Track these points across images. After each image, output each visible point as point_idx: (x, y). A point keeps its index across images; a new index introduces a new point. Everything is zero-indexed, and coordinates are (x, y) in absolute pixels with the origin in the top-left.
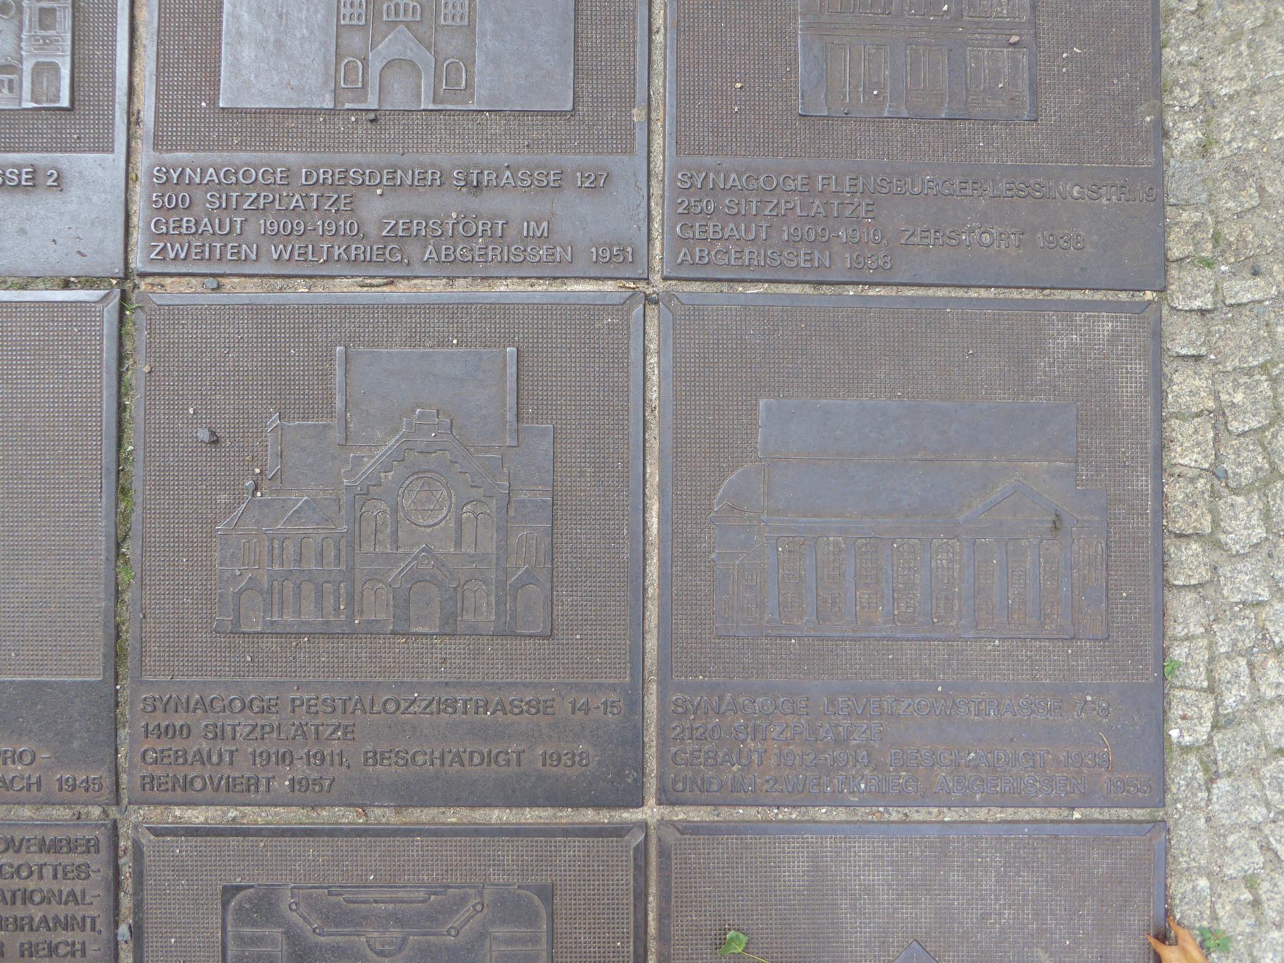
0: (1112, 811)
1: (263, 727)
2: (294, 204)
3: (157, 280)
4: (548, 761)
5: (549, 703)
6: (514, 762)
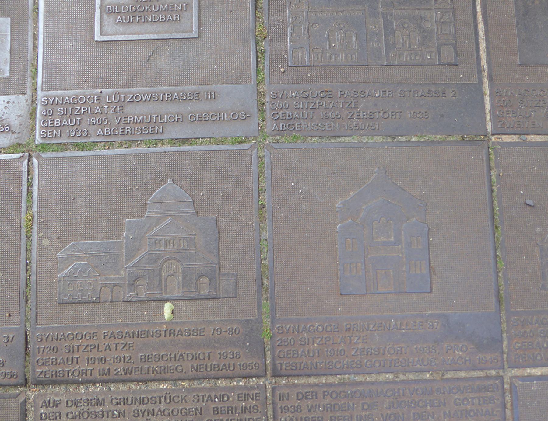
0: (373, 380)
1: (91, 346)
2: (96, 111)
3: (499, 136)
4: (116, 361)
5: (202, 331)
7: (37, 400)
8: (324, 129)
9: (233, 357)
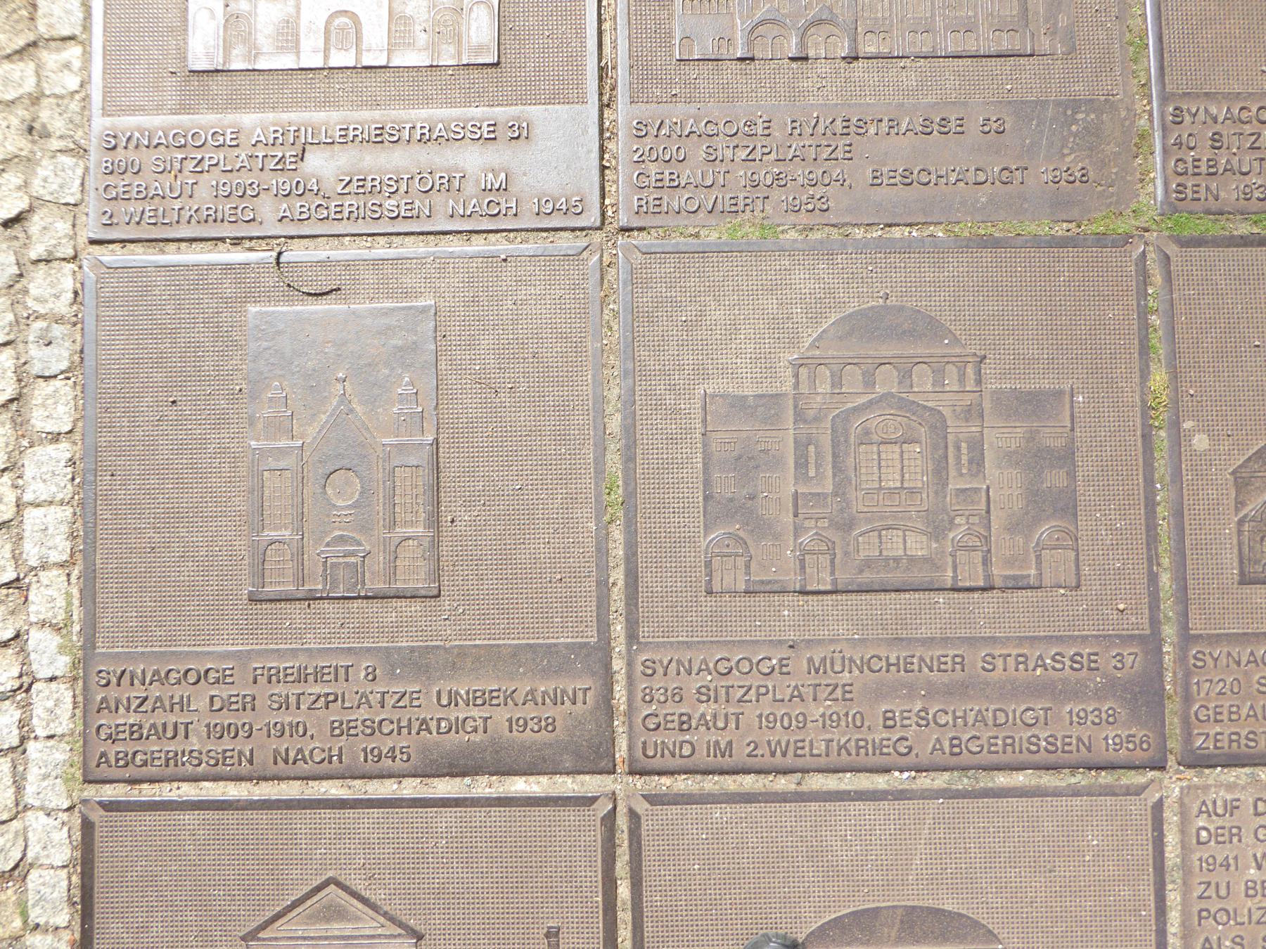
6: (481, 729)
7: (1186, 800)
8: (395, 215)
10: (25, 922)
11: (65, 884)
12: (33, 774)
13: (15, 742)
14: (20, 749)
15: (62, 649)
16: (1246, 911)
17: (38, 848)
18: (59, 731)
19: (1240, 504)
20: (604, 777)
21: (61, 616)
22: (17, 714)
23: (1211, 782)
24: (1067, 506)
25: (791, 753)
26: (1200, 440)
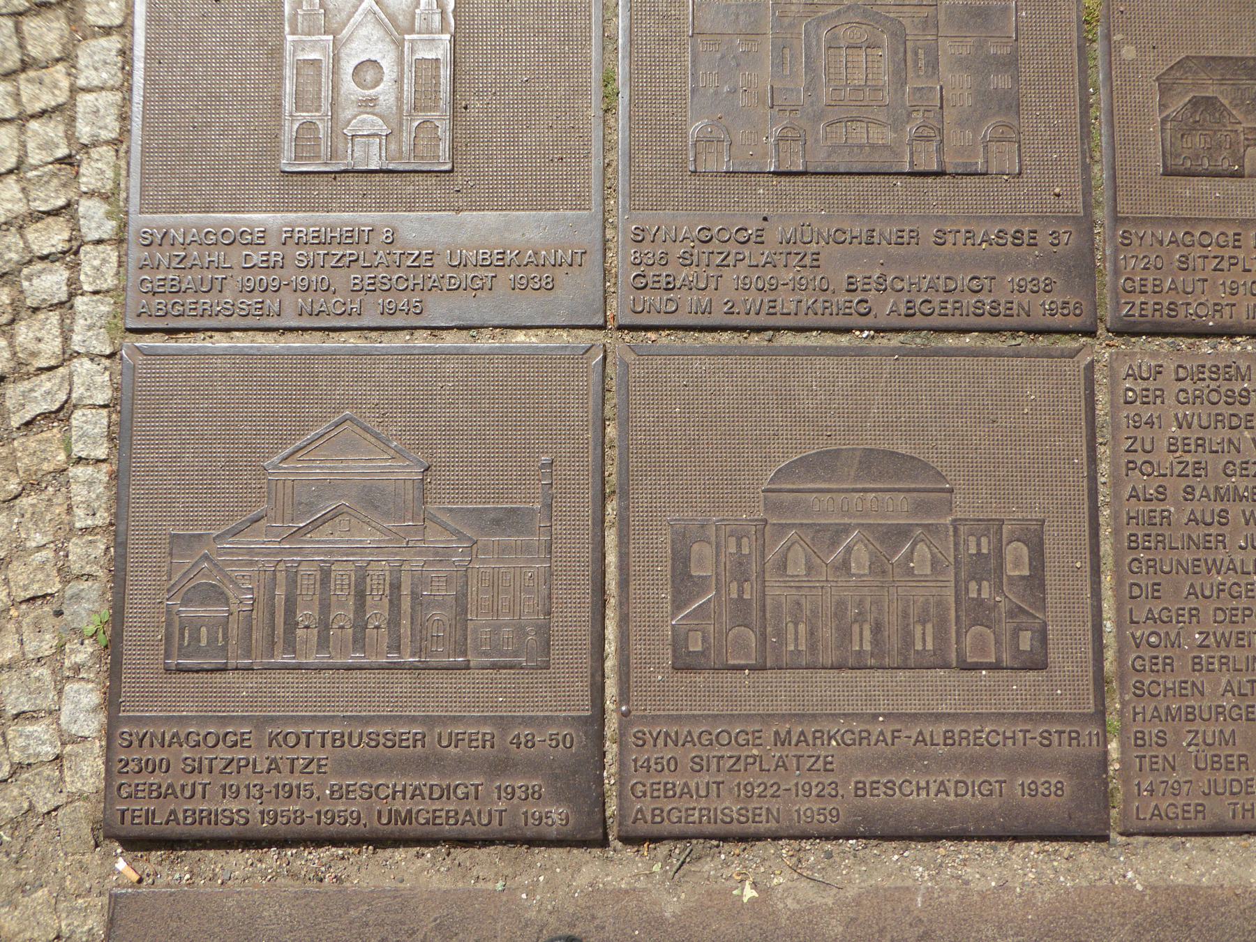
6: (472, 797)
7: (1115, 365)
9: (526, 798)
10: (69, 456)
11: (105, 421)
12: (80, 325)
13: (64, 297)
14: (68, 305)
15: (109, 216)
16: (1168, 465)
17: (82, 390)
18: (105, 287)
19: (1163, 106)
20: (597, 332)
21: (109, 185)
22: (66, 274)
23: (1137, 350)
24: (1011, 104)
25: (763, 312)
26: (1128, 51)
